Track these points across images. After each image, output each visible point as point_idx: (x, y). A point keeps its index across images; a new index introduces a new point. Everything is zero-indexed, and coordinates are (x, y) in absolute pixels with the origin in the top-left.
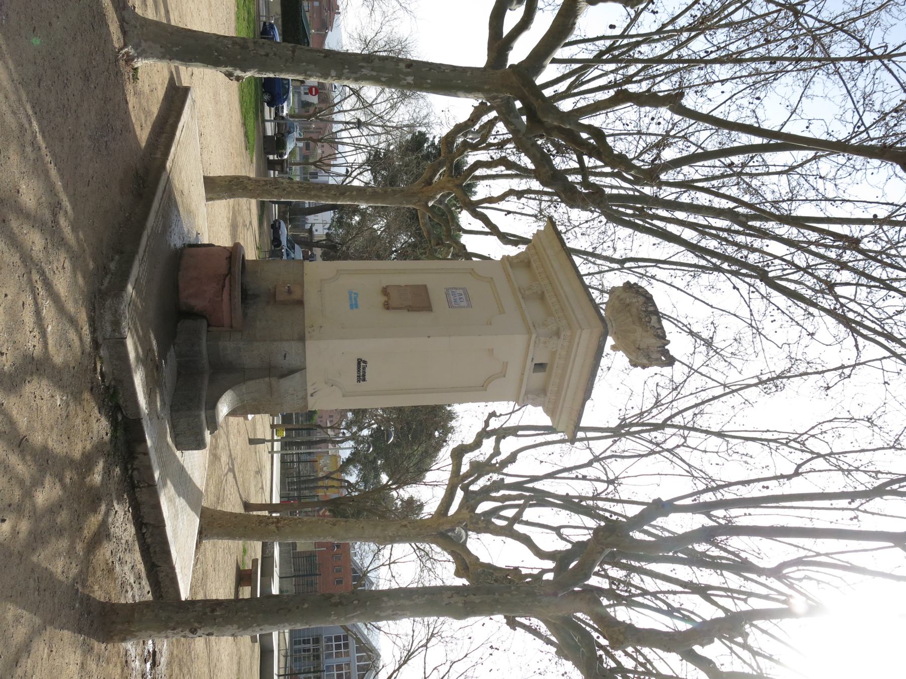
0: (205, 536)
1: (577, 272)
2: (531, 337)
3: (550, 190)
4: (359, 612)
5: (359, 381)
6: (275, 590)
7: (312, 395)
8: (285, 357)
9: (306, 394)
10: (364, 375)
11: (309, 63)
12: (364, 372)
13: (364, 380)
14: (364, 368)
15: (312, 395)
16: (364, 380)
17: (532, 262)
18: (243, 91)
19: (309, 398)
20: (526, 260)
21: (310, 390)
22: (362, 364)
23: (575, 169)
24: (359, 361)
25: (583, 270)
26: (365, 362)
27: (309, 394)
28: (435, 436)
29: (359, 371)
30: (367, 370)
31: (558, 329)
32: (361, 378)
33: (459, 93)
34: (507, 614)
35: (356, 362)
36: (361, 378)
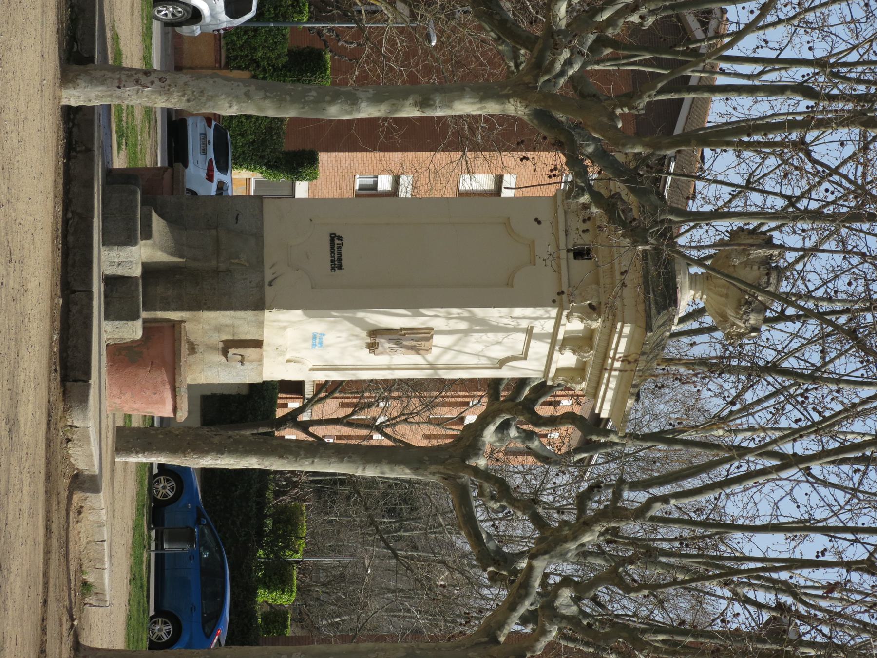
3: (700, 132)
5: (333, 269)
6: (159, 165)
7: (270, 284)
8: (237, 219)
9: (263, 283)
10: (340, 259)
12: (340, 254)
13: (340, 267)
14: (339, 248)
16: (340, 267)
19: (267, 287)
22: (337, 242)
23: (558, 312)
24: (333, 237)
26: (340, 238)
27: (266, 283)
28: (596, 149)
29: (332, 252)
30: (343, 249)
32: (337, 264)
33: (329, 457)
34: (523, 571)
35: (327, 239)
36: (337, 264)
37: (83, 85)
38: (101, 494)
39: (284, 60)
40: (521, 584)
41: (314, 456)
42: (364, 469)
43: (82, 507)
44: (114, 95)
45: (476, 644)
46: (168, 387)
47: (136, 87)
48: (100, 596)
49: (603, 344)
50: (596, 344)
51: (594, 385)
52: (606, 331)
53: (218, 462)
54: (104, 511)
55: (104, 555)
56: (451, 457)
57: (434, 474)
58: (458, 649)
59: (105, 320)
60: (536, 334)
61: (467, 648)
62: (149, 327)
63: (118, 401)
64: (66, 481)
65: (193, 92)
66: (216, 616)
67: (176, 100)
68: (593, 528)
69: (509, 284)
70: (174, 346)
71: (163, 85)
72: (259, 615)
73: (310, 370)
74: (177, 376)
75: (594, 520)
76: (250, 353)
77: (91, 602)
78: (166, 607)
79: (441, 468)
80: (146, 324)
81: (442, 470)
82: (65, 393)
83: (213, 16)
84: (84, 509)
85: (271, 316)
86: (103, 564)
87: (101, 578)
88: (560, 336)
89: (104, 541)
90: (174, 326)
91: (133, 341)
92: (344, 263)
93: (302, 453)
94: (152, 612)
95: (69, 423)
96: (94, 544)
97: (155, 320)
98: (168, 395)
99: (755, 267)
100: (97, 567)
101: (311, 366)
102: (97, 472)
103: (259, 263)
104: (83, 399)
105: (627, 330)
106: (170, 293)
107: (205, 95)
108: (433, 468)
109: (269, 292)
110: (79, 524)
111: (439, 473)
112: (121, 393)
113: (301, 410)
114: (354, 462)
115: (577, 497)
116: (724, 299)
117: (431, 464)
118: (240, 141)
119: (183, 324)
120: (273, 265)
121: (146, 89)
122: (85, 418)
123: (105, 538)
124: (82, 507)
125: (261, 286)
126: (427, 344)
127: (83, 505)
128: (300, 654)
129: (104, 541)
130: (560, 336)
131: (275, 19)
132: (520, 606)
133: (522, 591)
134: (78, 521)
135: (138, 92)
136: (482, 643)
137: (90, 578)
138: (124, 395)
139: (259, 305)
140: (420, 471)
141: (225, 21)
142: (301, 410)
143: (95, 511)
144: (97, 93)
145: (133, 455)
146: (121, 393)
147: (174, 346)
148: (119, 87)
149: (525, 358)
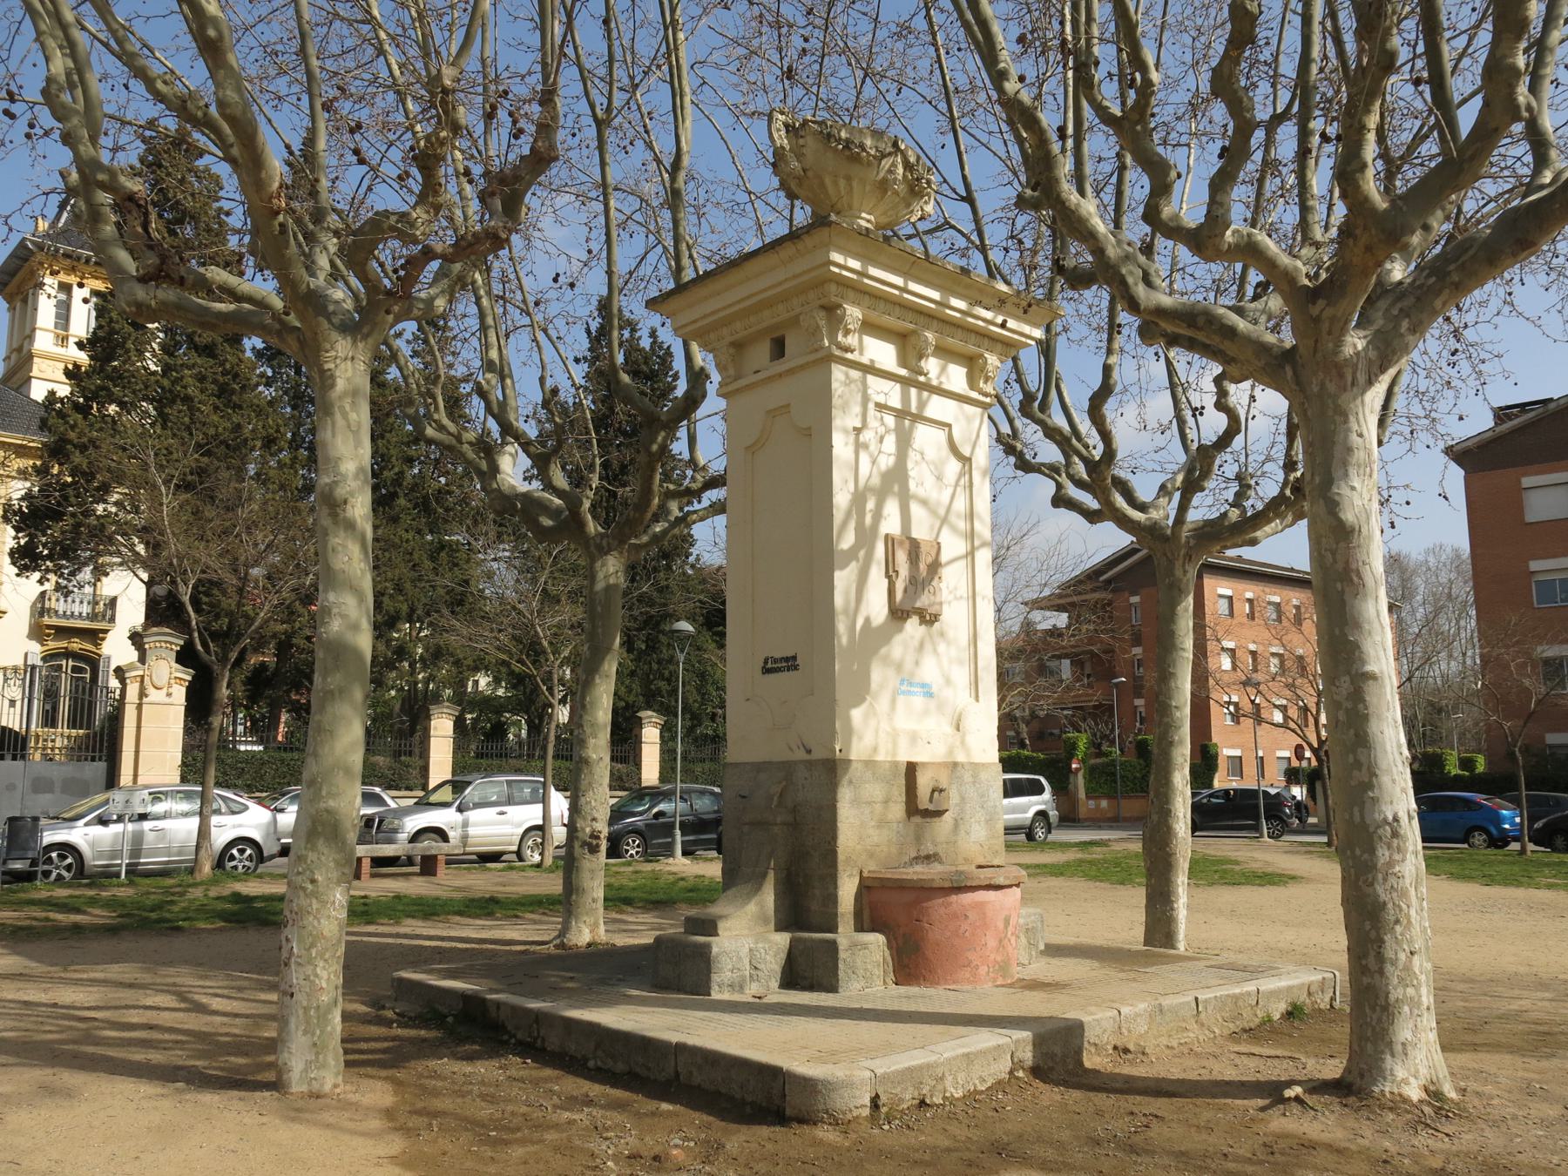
0: (1362, 1076)
1: (671, 293)
2: (837, 357)
4: (1478, 661)
5: (796, 668)
7: (809, 752)
8: (744, 797)
10: (787, 659)
11: (109, 874)
13: (794, 658)
14: (775, 661)
15: (809, 752)
16: (794, 658)
17: (737, 337)
18: (298, 399)
20: (732, 351)
21: (800, 755)
24: (767, 671)
25: (693, 275)
26: (766, 662)
30: (778, 655)
31: (823, 307)
32: (790, 663)
33: (1169, 689)
36: (790, 663)
37: (286, 1055)
38: (1086, 1019)
39: (1141, 761)
40: (1189, 326)
41: (1170, 706)
42: (1183, 649)
43: (1115, 1048)
44: (305, 1003)
45: (1298, 383)
46: (954, 898)
47: (293, 967)
48: (1313, 989)
49: (910, 316)
50: (912, 326)
51: (986, 341)
52: (867, 301)
53: (1181, 815)
54: (1125, 1010)
55: (1228, 996)
56: (1165, 554)
57: (1185, 572)
58: (1309, 413)
59: (832, 988)
60: (903, 404)
61: (1306, 397)
62: (867, 919)
63: (983, 970)
64: (1050, 1095)
65: (299, 873)
66: (1467, 801)
67: (314, 901)
68: (1073, 208)
69: (807, 433)
70: (891, 888)
71: (291, 922)
72: (1460, 772)
73: (977, 700)
74: (935, 885)
75: (1059, 207)
76: (924, 782)
77: (1327, 999)
78: (1460, 835)
79: (1178, 564)
80: (865, 927)
81: (1181, 562)
82: (801, 1121)
83: (1045, 803)
84: (1119, 1044)
85: (858, 750)
86: (1249, 994)
87: (1275, 994)
88: (903, 372)
89: (1196, 999)
90: (868, 888)
91: (890, 947)
92: (789, 654)
93: (1166, 720)
94: (1466, 846)
95: (866, 1112)
96: (1203, 1015)
97: (858, 914)
98: (967, 898)
99: (801, 141)
100: (1254, 1003)
101: (972, 700)
102: (1025, 1035)
103: (787, 768)
104: (808, 1085)
105: (836, 257)
106: (817, 892)
107: (304, 852)
108: (1178, 573)
109: (818, 754)
110: (1147, 1050)
111: (1184, 565)
112: (969, 965)
113: (1310, 745)
114: (1174, 661)
115: (1073, 287)
116: (855, 184)
117: (1173, 575)
118: (1403, 784)
119: (865, 874)
120: (791, 749)
121: (295, 950)
122: (849, 1084)
123: (1190, 998)
124: (1115, 1048)
125: (810, 764)
126: (924, 549)
127: (1110, 1047)
128: (1334, 688)
129: (1196, 999)
130: (903, 372)
131: (1115, 767)
132: (1225, 321)
133: (1201, 321)
134: (1143, 1053)
135: (300, 964)
136: (1295, 373)
137: (1278, 1009)
138: (970, 962)
139: (831, 770)
140: (1182, 586)
141: (1047, 795)
142: (1310, 745)
143: (1123, 1025)
144: (300, 1033)
145: (1175, 913)
146: (969, 965)
147: (891, 888)
148: (292, 995)
149: (949, 426)
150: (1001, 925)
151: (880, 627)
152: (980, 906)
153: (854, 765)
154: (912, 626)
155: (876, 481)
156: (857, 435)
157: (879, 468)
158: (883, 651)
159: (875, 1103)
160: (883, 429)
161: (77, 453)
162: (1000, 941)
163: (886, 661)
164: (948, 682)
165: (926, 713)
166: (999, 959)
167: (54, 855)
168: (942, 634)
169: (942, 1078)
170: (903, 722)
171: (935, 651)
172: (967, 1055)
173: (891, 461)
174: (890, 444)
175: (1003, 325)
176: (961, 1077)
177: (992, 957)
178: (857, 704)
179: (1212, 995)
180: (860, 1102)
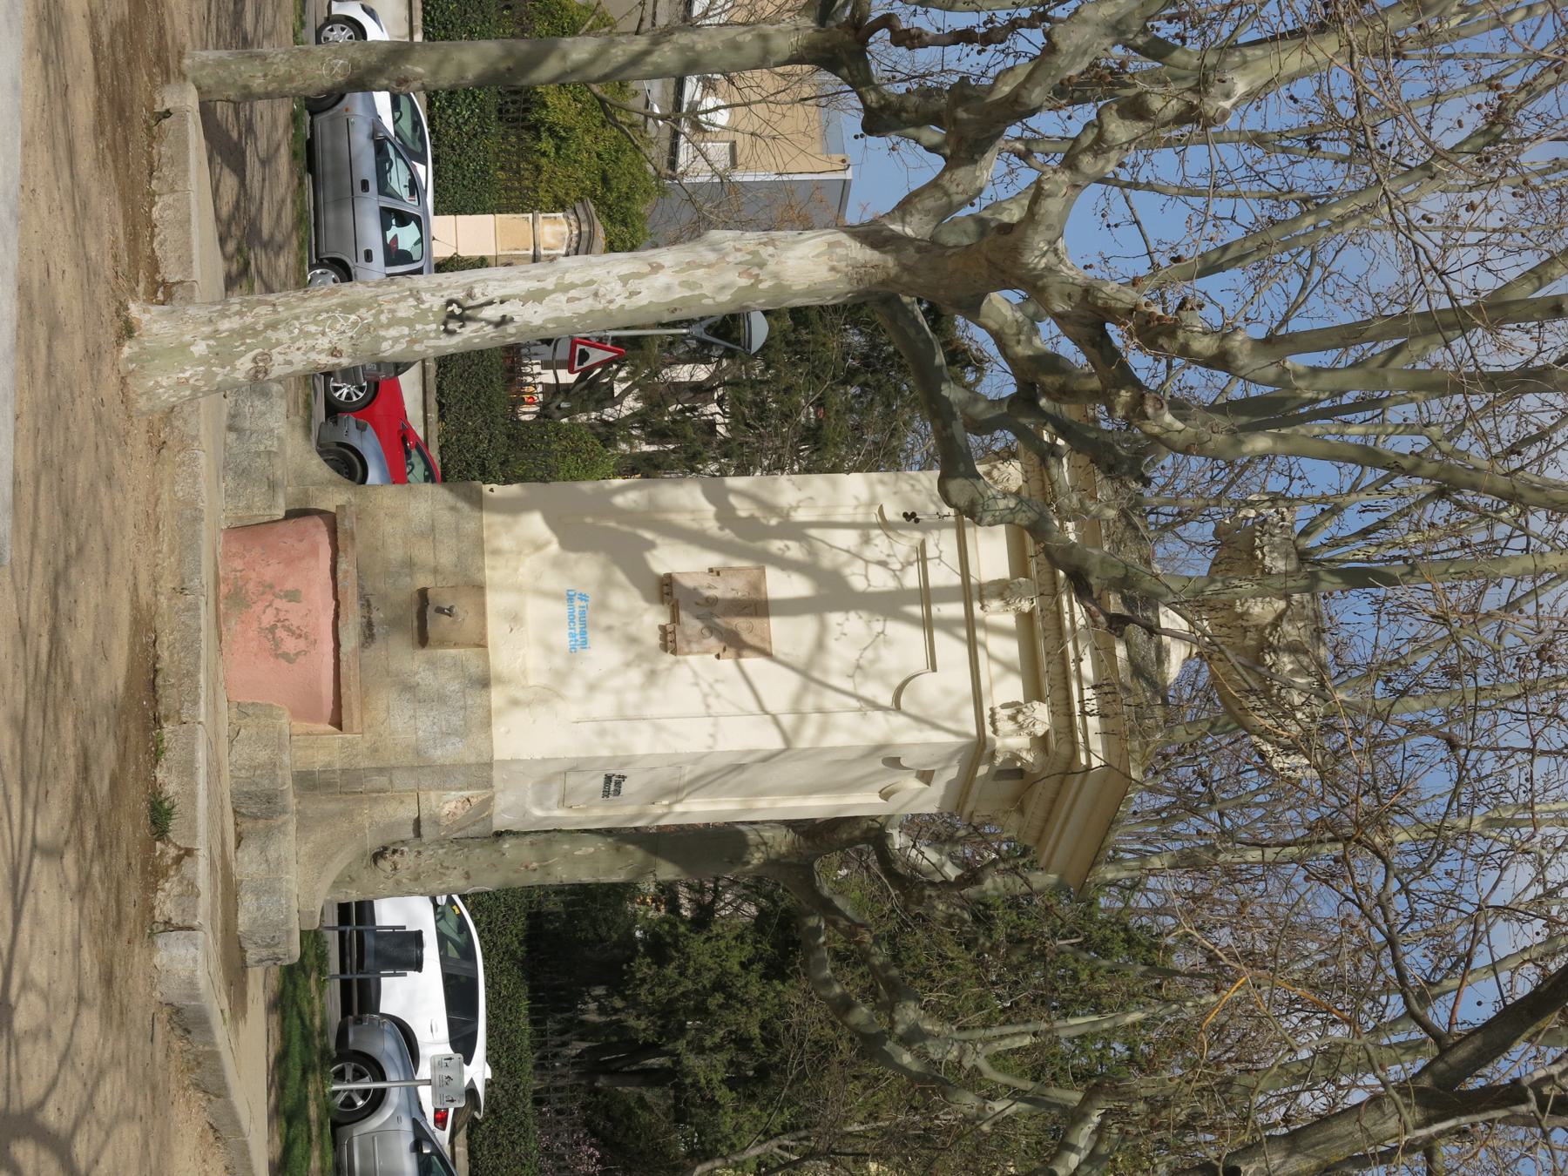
137: (170, 784)
150: (290, 585)
151: (645, 565)
152: (314, 552)
153: (477, 514)
154: (653, 618)
155: (826, 561)
156: (877, 526)
157: (847, 564)
158: (620, 576)
159: (167, 114)
160: (897, 566)
161: (884, 652)
162: (271, 587)
163: (607, 583)
164: (592, 687)
165: (549, 649)
166: (251, 586)
167: (360, 1103)
168: (652, 675)
169: (173, 191)
170: (537, 611)
171: (628, 665)
172: (189, 221)
173: (858, 583)
174: (881, 581)
175: (1084, 713)
176: (169, 214)
177: (253, 575)
178: (553, 523)
179: (203, 622)
180: (167, 99)
